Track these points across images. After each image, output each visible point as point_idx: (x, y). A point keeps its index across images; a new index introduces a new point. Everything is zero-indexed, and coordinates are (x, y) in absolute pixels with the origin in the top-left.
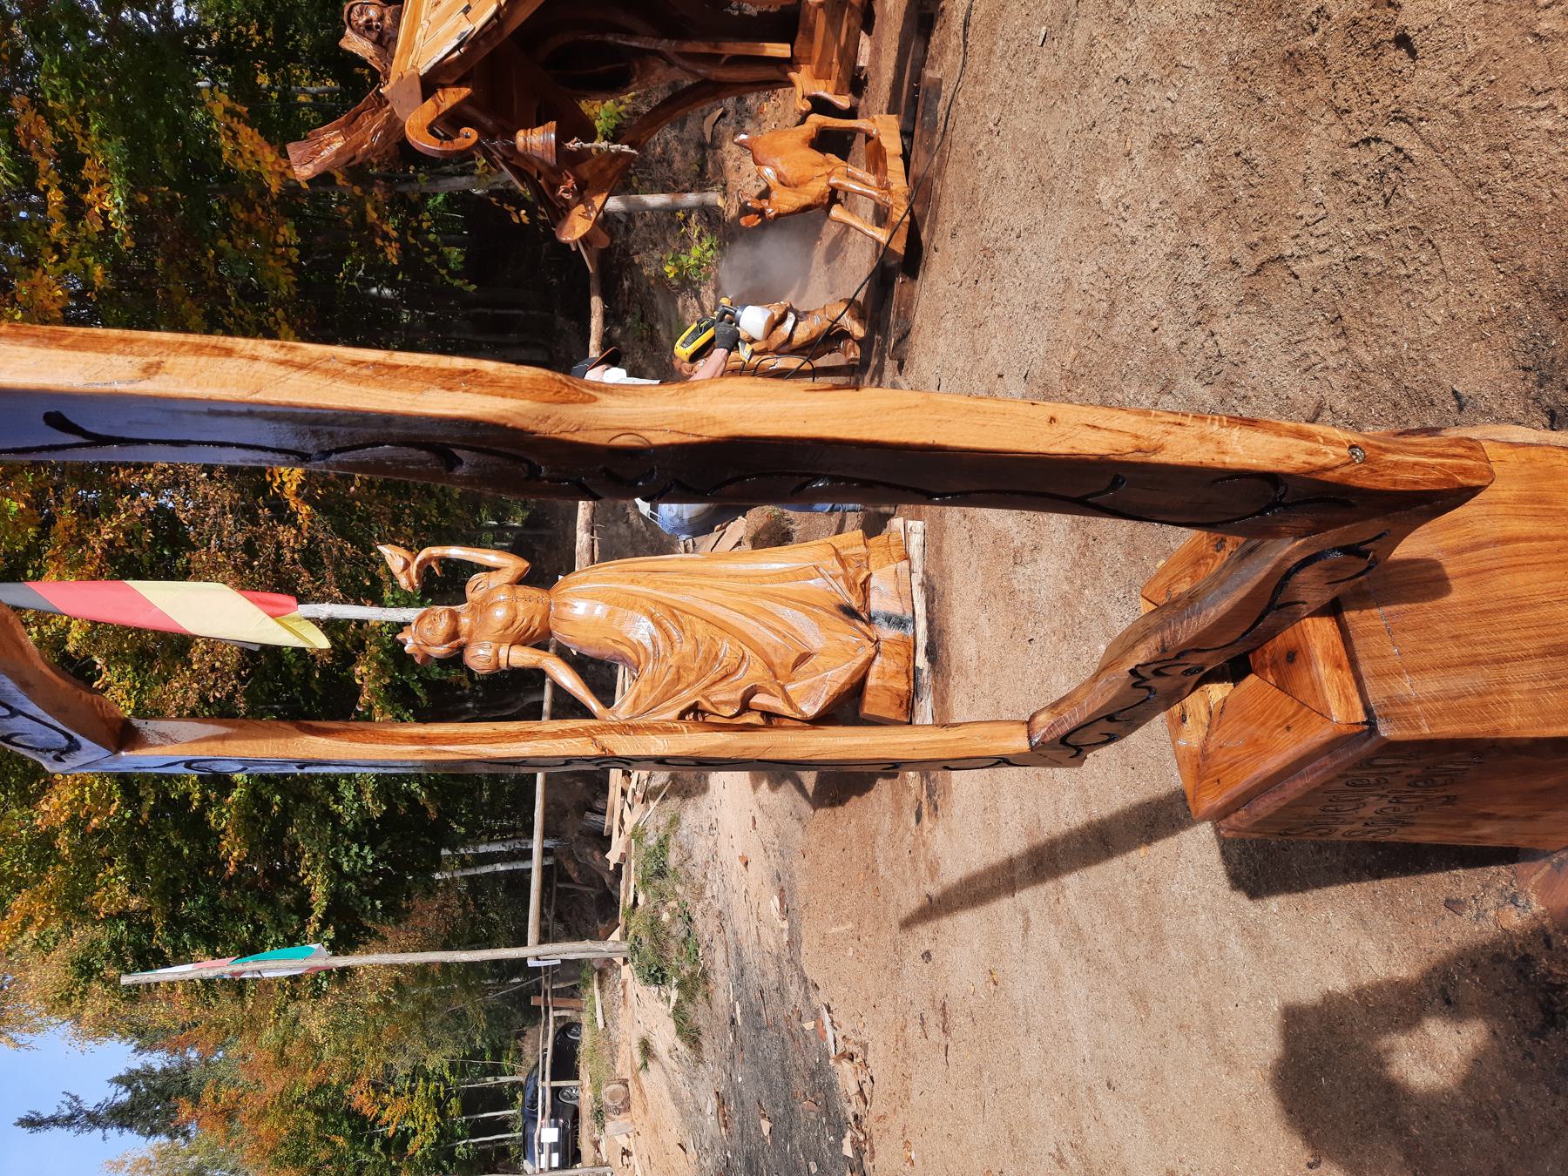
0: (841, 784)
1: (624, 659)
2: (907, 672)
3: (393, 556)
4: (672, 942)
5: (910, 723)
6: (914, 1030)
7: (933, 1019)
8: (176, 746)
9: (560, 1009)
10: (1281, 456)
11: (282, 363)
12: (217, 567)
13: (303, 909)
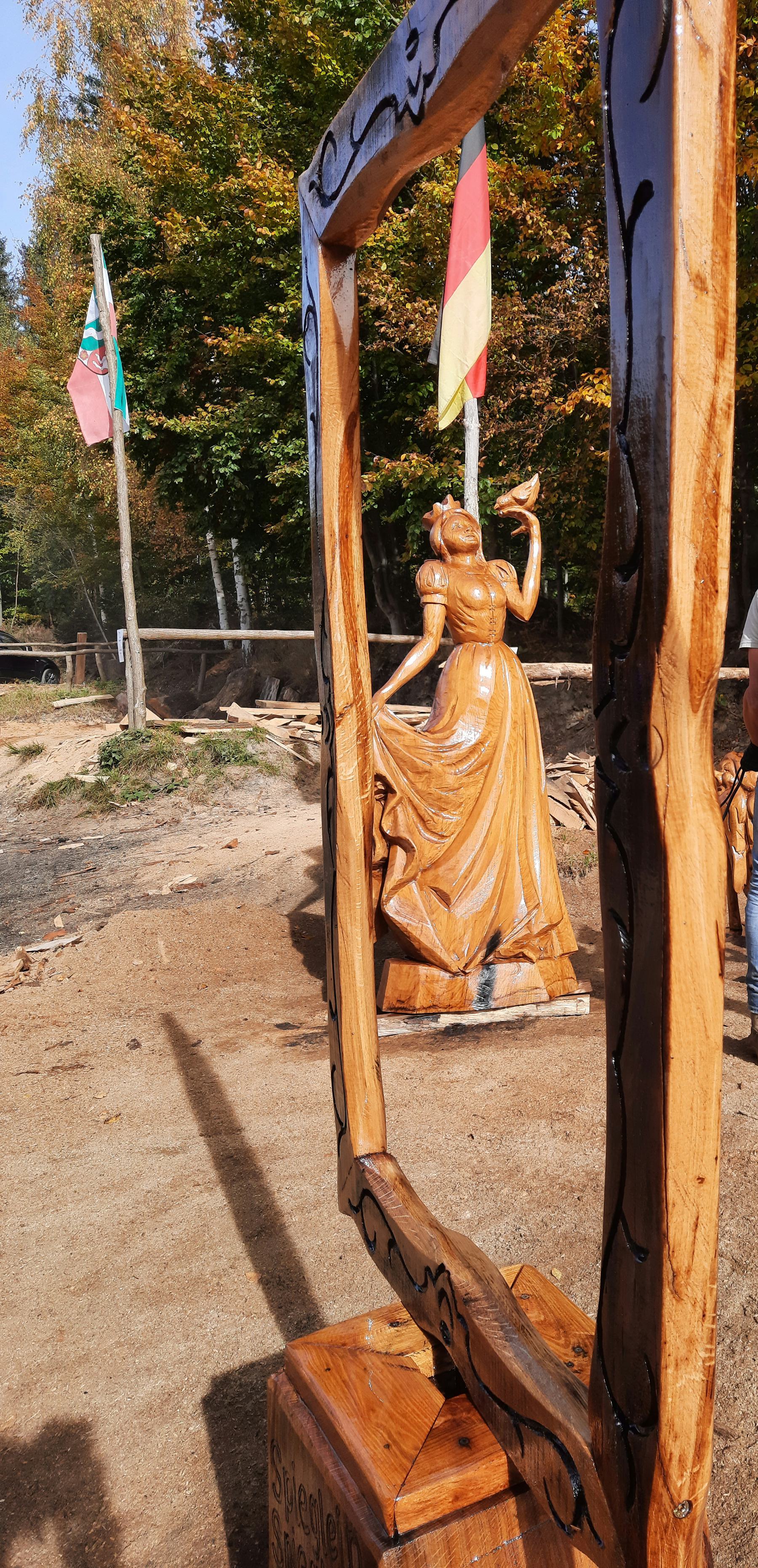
0: (314, 941)
1: (436, 717)
2: (434, 1006)
3: (528, 489)
4: (146, 773)
5: (379, 1011)
6: (54, 1035)
7: (66, 1056)
8: (328, 295)
9: (74, 661)
10: (677, 1428)
11: (713, 406)
12: (508, 325)
13: (174, 408)
